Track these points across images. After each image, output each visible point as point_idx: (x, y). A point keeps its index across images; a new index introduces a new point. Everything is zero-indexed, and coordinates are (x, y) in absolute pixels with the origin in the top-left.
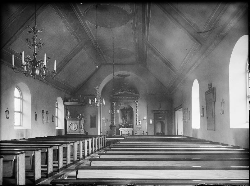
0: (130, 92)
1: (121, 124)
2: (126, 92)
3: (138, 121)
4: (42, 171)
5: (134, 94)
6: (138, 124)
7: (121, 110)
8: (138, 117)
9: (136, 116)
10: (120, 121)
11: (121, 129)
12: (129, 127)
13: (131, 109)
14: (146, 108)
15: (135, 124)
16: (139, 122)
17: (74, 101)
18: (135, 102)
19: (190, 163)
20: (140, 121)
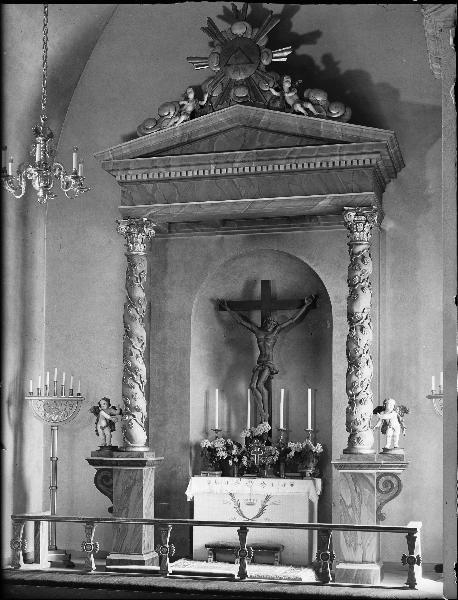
0: (286, 108)
1: (206, 443)
2: (252, 111)
3: (365, 411)
4: (238, 476)
5: (325, 126)
6: (367, 444)
7: (221, 305)
8: (366, 372)
9: (353, 362)
10: (205, 407)
11: (213, 498)
12: (289, 465)
13: (312, 305)
14: (441, 286)
15: (340, 439)
16: (386, 425)
17: (132, 312)
18: (339, 211)
19: (351, 340)
20: (391, 415)
